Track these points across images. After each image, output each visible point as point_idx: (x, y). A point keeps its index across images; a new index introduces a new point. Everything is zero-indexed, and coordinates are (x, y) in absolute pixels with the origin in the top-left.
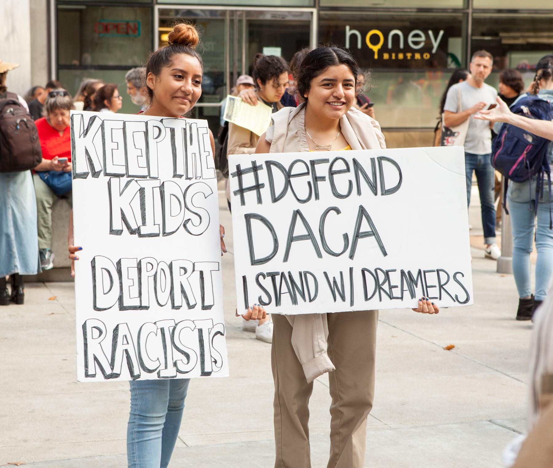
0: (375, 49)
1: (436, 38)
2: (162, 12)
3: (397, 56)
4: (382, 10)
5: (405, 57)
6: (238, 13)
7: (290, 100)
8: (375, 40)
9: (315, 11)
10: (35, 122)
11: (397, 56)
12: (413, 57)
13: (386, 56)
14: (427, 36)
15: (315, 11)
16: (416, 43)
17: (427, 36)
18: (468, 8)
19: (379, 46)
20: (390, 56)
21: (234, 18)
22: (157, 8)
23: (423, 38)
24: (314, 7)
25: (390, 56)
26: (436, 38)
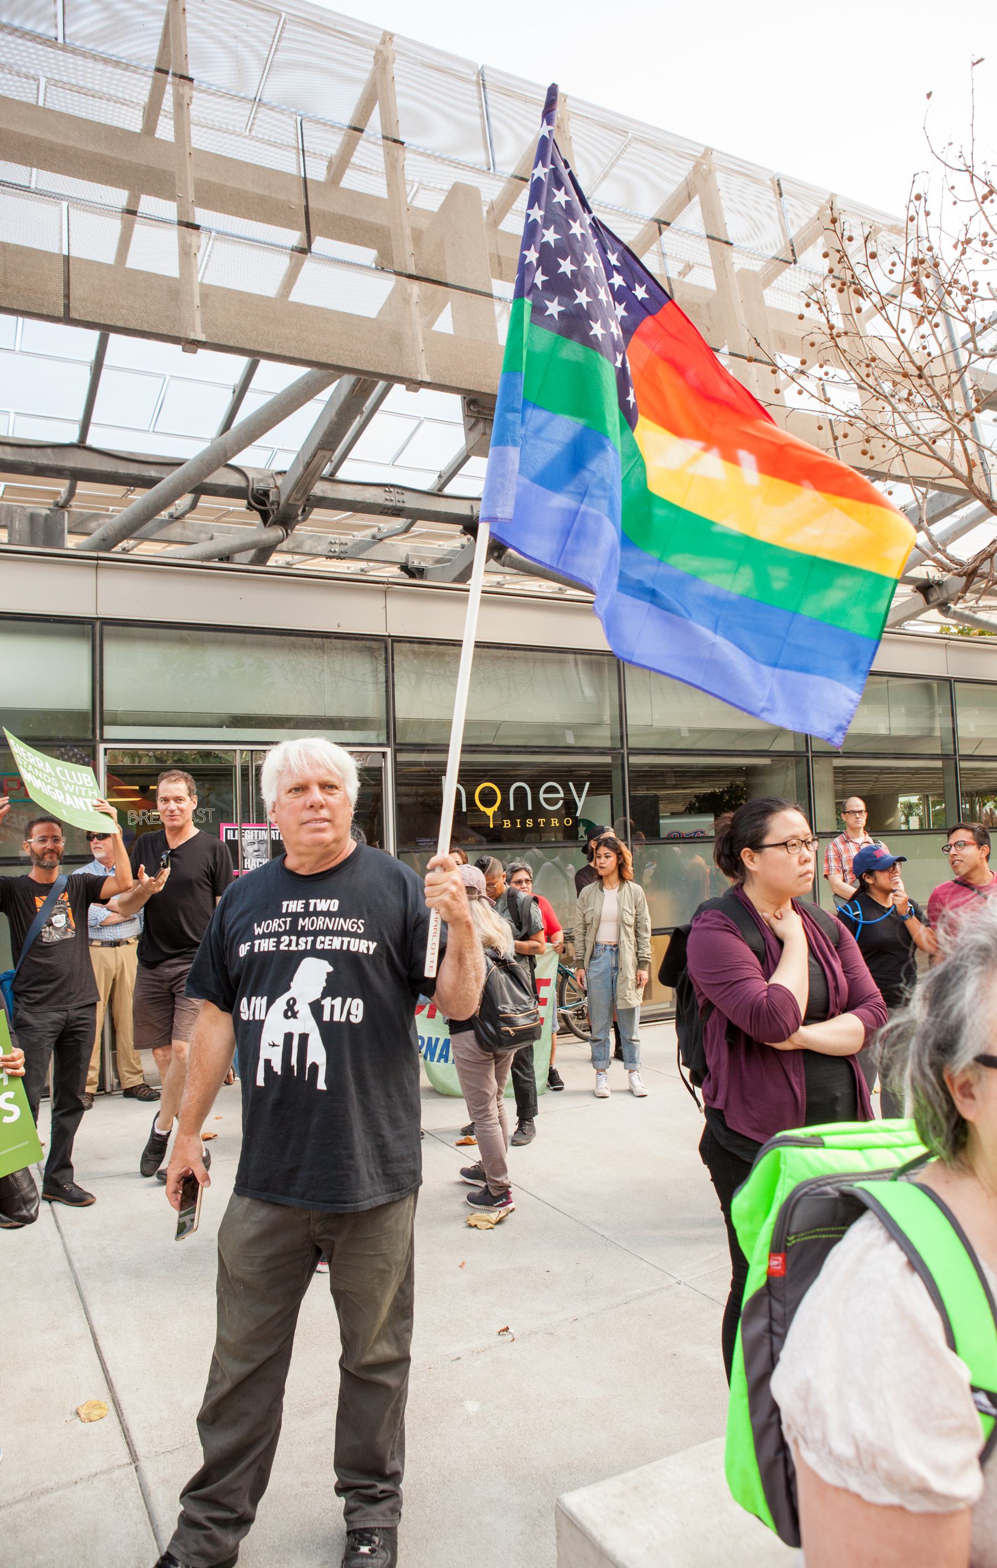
0: (490, 811)
1: (580, 797)
2: (48, 1096)
3: (523, 823)
4: (497, 749)
5: (536, 824)
6: (850, 480)
7: (910, 966)
8: (488, 799)
9: (388, 750)
10: (190, 179)
11: (523, 823)
12: (548, 823)
13: (507, 824)
14: (567, 790)
15: (388, 750)
16: (550, 802)
17: (567, 790)
18: (622, 747)
19: (495, 808)
20: (514, 823)
21: (172, 802)
22: (102, 747)
23: (542, 796)
24: (387, 745)
25: (514, 823)
26: (580, 797)
